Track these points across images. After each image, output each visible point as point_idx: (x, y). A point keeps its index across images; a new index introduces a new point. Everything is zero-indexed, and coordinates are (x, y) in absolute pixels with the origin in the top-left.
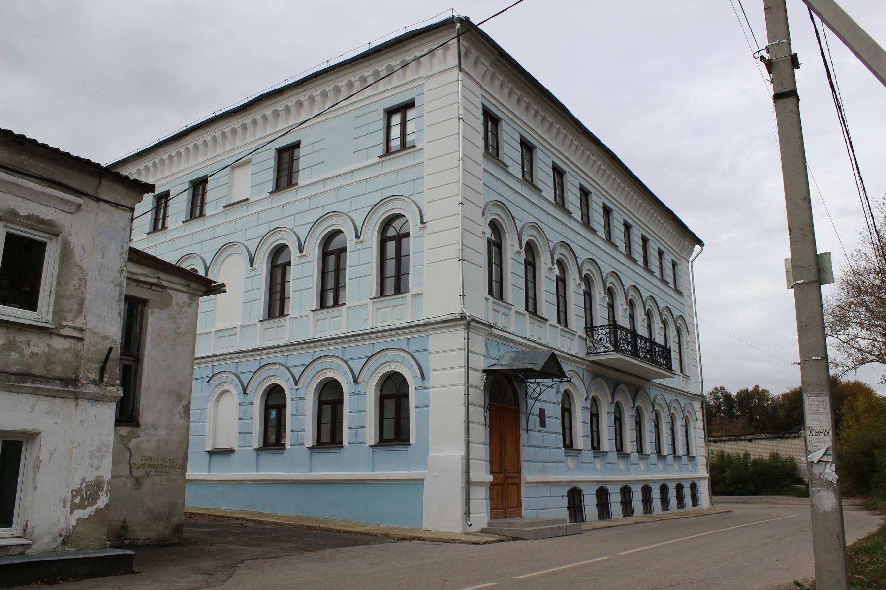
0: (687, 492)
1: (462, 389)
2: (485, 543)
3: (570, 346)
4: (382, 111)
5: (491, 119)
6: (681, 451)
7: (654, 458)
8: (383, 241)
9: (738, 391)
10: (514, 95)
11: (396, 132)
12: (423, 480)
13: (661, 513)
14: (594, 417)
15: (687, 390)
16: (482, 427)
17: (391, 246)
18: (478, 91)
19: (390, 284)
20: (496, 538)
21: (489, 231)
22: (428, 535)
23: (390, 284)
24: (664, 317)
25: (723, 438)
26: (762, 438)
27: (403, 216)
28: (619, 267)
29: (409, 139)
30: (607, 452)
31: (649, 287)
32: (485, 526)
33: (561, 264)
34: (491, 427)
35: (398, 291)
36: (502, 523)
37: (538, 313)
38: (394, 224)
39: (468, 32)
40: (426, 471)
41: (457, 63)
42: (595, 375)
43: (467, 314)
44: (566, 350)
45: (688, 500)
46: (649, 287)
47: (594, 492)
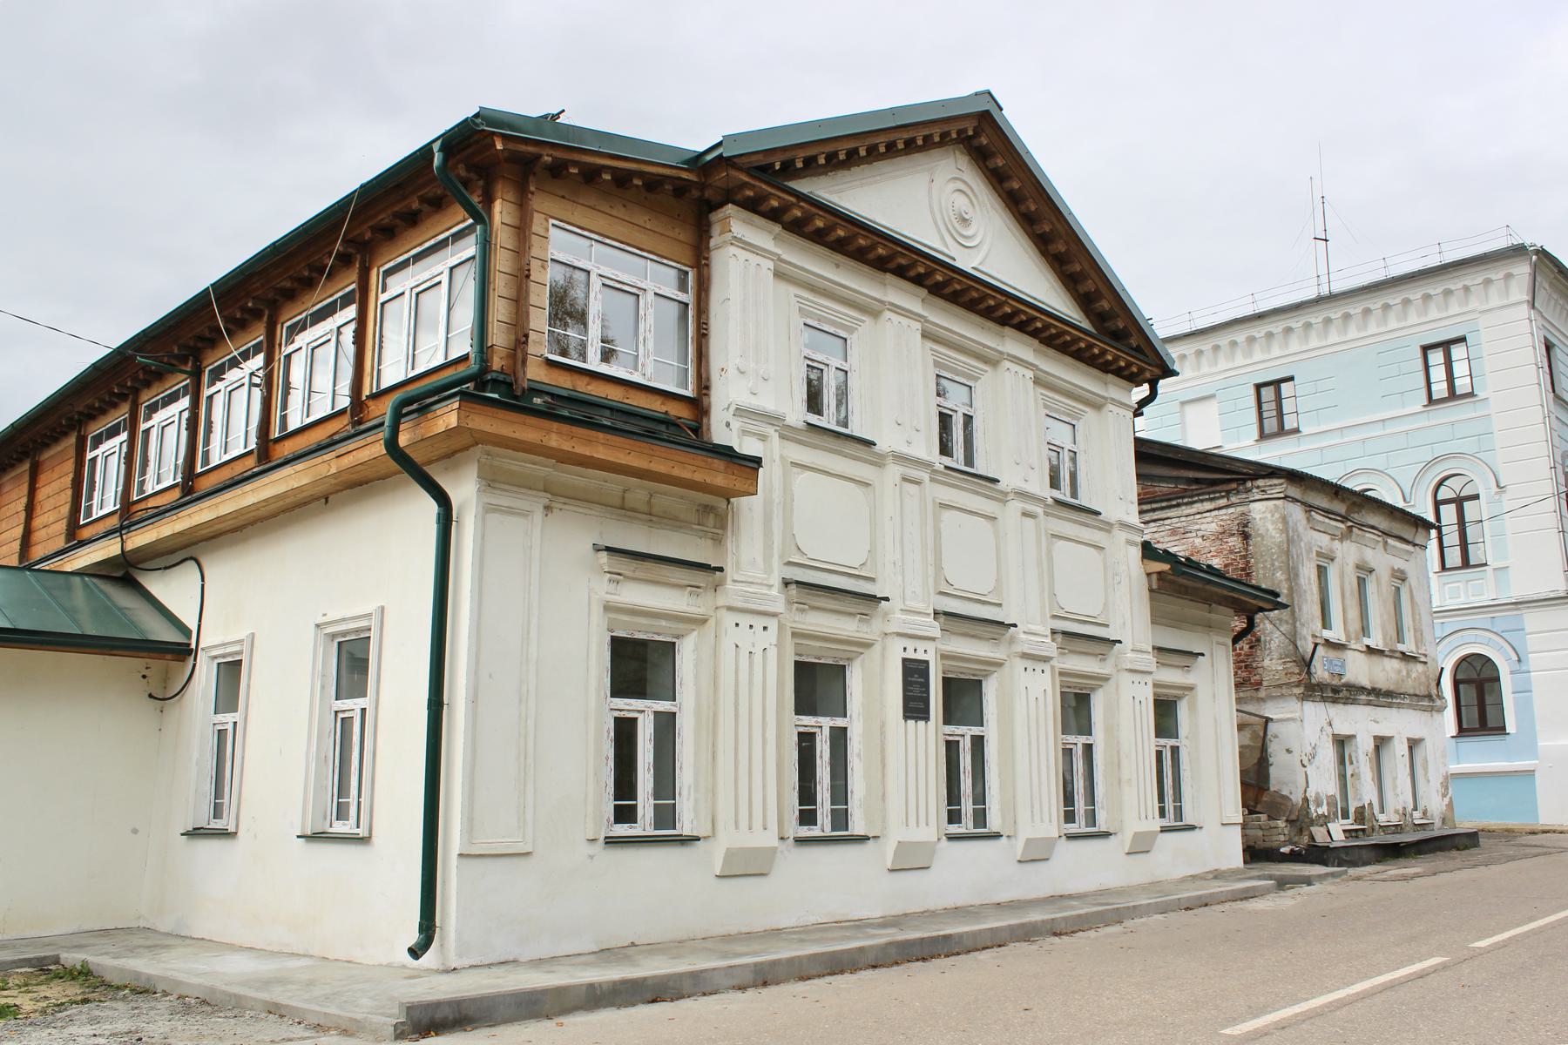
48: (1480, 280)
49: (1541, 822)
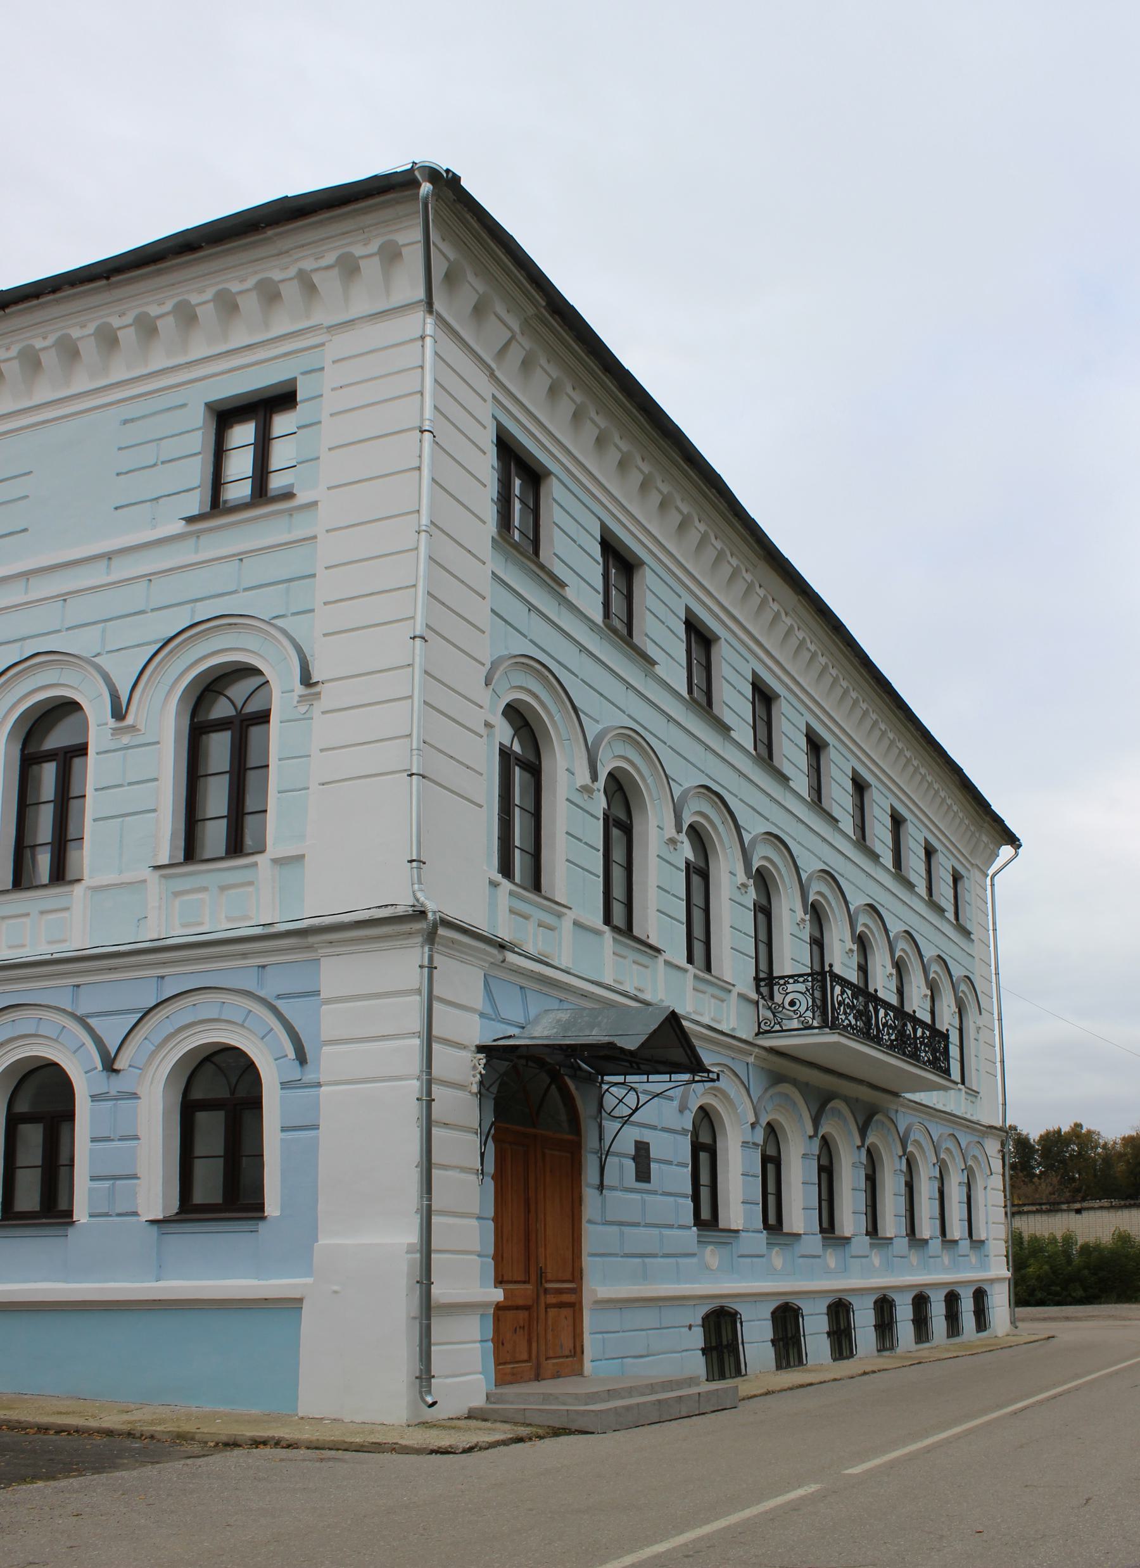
0: (967, 1306)
1: (414, 1087)
2: (470, 1450)
3: (718, 1011)
4: (201, 409)
5: (520, 470)
6: (957, 1230)
7: (901, 1244)
8: (198, 731)
9: (1043, 1132)
10: (589, 425)
11: (240, 464)
12: (301, 1300)
13: (913, 1346)
14: (772, 1163)
15: (974, 1118)
16: (473, 1179)
17: (219, 746)
18: (487, 387)
19: (215, 835)
20: (502, 1432)
21: (504, 733)
22: (307, 1434)
23: (215, 835)
24: (932, 975)
25: (1026, 1209)
26: (1101, 1208)
27: (257, 672)
28: (838, 865)
29: (276, 483)
30: (799, 1235)
31: (903, 913)
32: (479, 1402)
33: (697, 835)
34: (499, 1177)
35: (236, 846)
36: (529, 1396)
37: (636, 932)
38: (229, 693)
39: (442, 204)
40: (309, 1280)
41: (421, 294)
42: (777, 1078)
43: (430, 906)
44: (706, 1020)
45: (968, 1319)
46: (903, 913)
47: (769, 1316)
48: (330, 258)
49: (305, 1408)
